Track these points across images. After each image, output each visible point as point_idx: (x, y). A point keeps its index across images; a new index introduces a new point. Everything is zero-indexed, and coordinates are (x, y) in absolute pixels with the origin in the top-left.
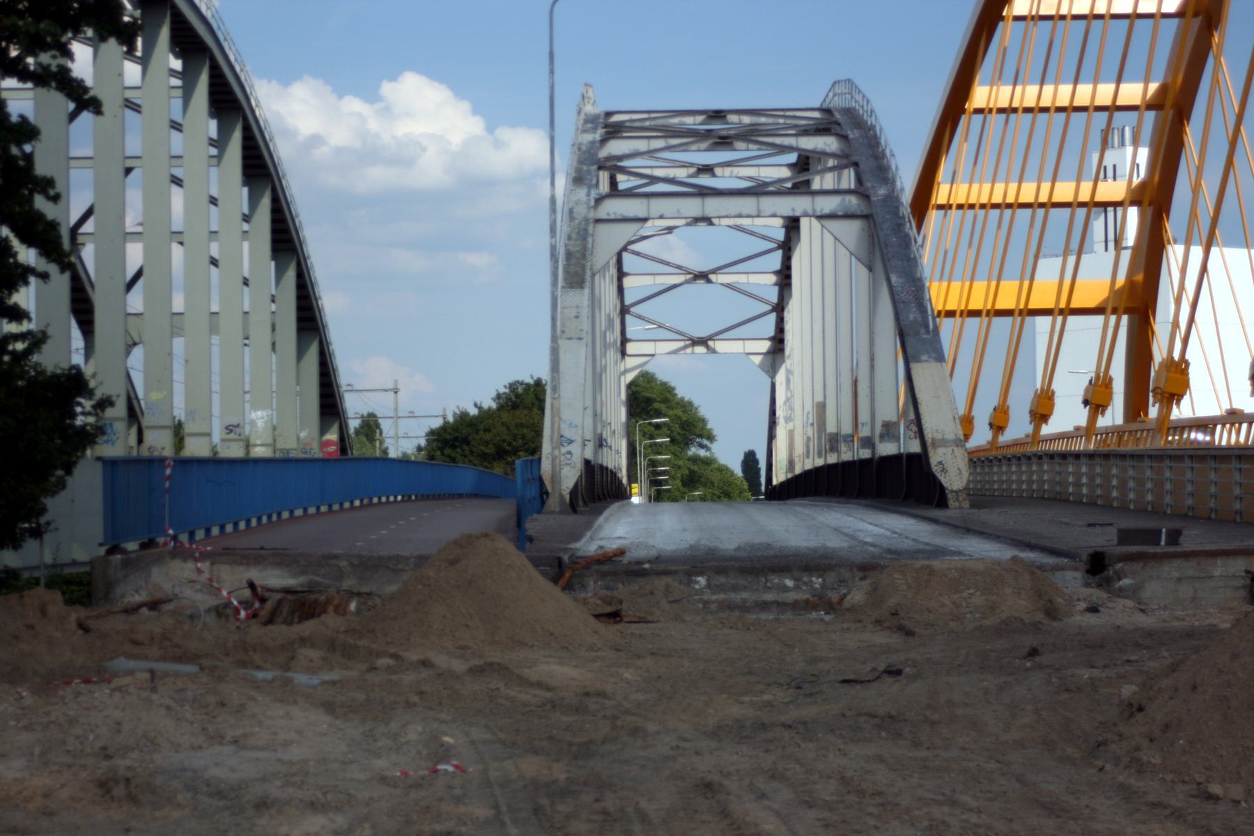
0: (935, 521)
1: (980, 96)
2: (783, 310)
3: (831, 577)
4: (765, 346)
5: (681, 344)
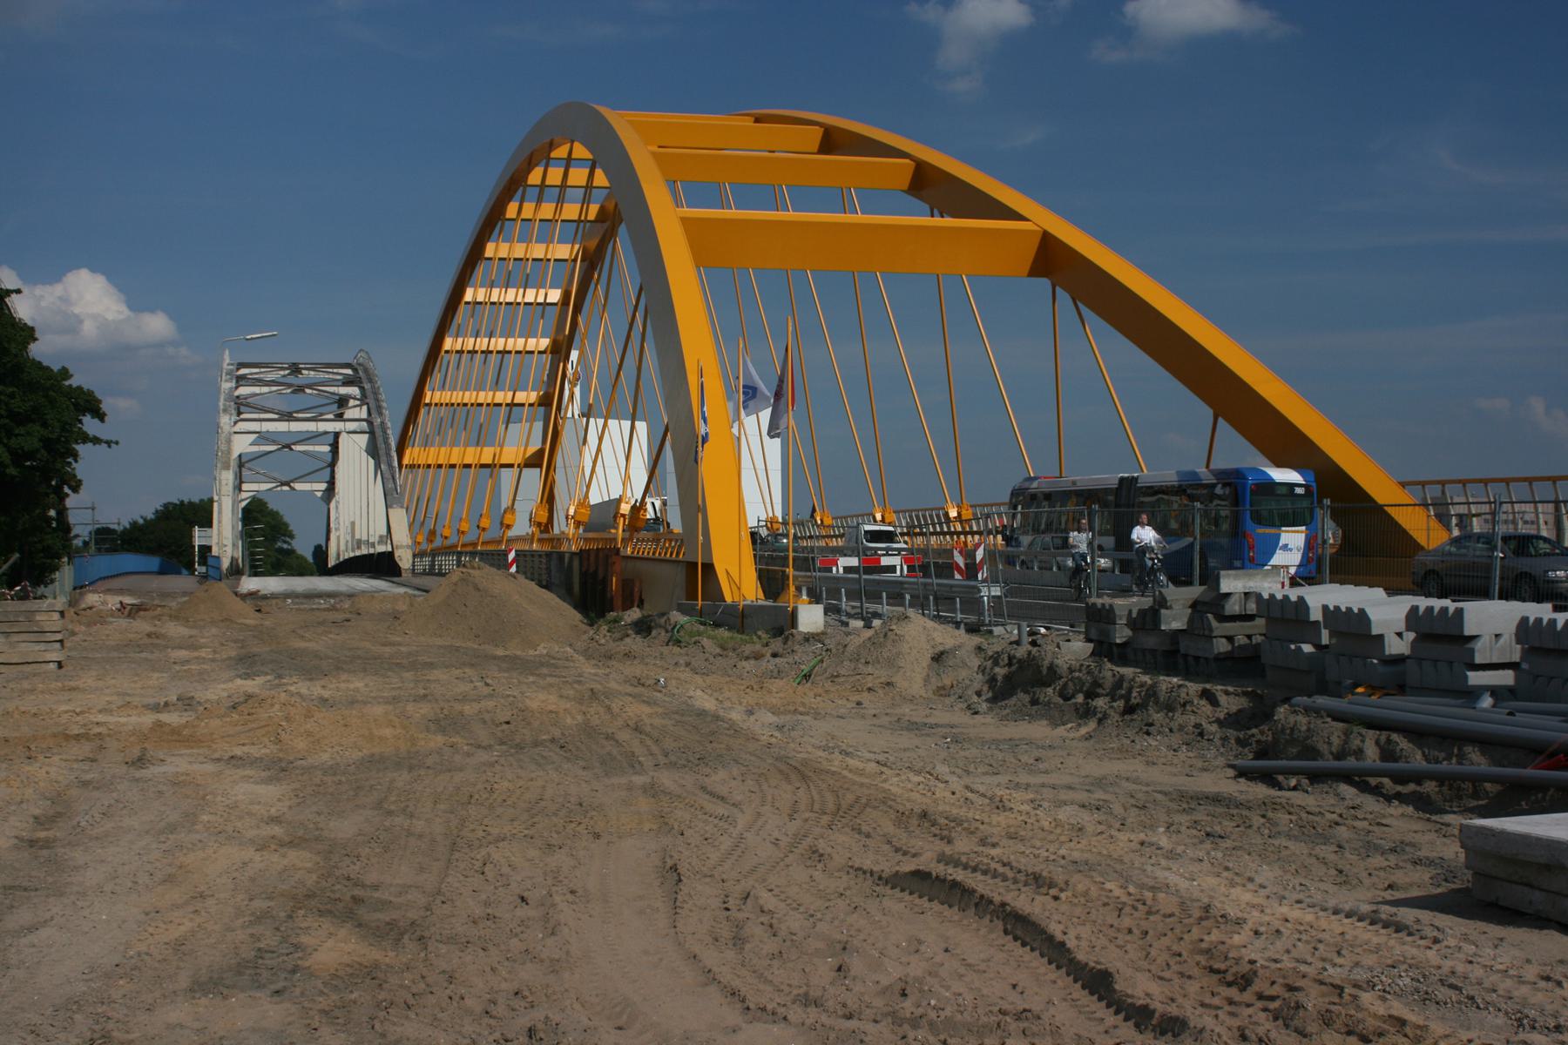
0: (393, 582)
1: (448, 343)
2: (334, 466)
3: (337, 600)
4: (323, 486)
5: (274, 485)
